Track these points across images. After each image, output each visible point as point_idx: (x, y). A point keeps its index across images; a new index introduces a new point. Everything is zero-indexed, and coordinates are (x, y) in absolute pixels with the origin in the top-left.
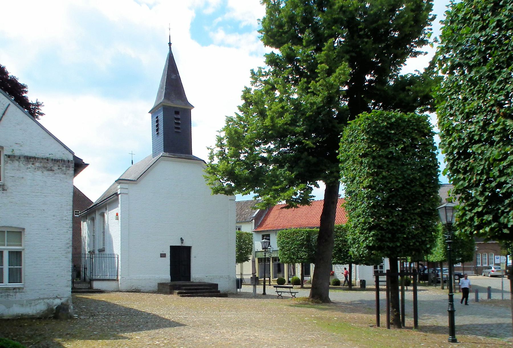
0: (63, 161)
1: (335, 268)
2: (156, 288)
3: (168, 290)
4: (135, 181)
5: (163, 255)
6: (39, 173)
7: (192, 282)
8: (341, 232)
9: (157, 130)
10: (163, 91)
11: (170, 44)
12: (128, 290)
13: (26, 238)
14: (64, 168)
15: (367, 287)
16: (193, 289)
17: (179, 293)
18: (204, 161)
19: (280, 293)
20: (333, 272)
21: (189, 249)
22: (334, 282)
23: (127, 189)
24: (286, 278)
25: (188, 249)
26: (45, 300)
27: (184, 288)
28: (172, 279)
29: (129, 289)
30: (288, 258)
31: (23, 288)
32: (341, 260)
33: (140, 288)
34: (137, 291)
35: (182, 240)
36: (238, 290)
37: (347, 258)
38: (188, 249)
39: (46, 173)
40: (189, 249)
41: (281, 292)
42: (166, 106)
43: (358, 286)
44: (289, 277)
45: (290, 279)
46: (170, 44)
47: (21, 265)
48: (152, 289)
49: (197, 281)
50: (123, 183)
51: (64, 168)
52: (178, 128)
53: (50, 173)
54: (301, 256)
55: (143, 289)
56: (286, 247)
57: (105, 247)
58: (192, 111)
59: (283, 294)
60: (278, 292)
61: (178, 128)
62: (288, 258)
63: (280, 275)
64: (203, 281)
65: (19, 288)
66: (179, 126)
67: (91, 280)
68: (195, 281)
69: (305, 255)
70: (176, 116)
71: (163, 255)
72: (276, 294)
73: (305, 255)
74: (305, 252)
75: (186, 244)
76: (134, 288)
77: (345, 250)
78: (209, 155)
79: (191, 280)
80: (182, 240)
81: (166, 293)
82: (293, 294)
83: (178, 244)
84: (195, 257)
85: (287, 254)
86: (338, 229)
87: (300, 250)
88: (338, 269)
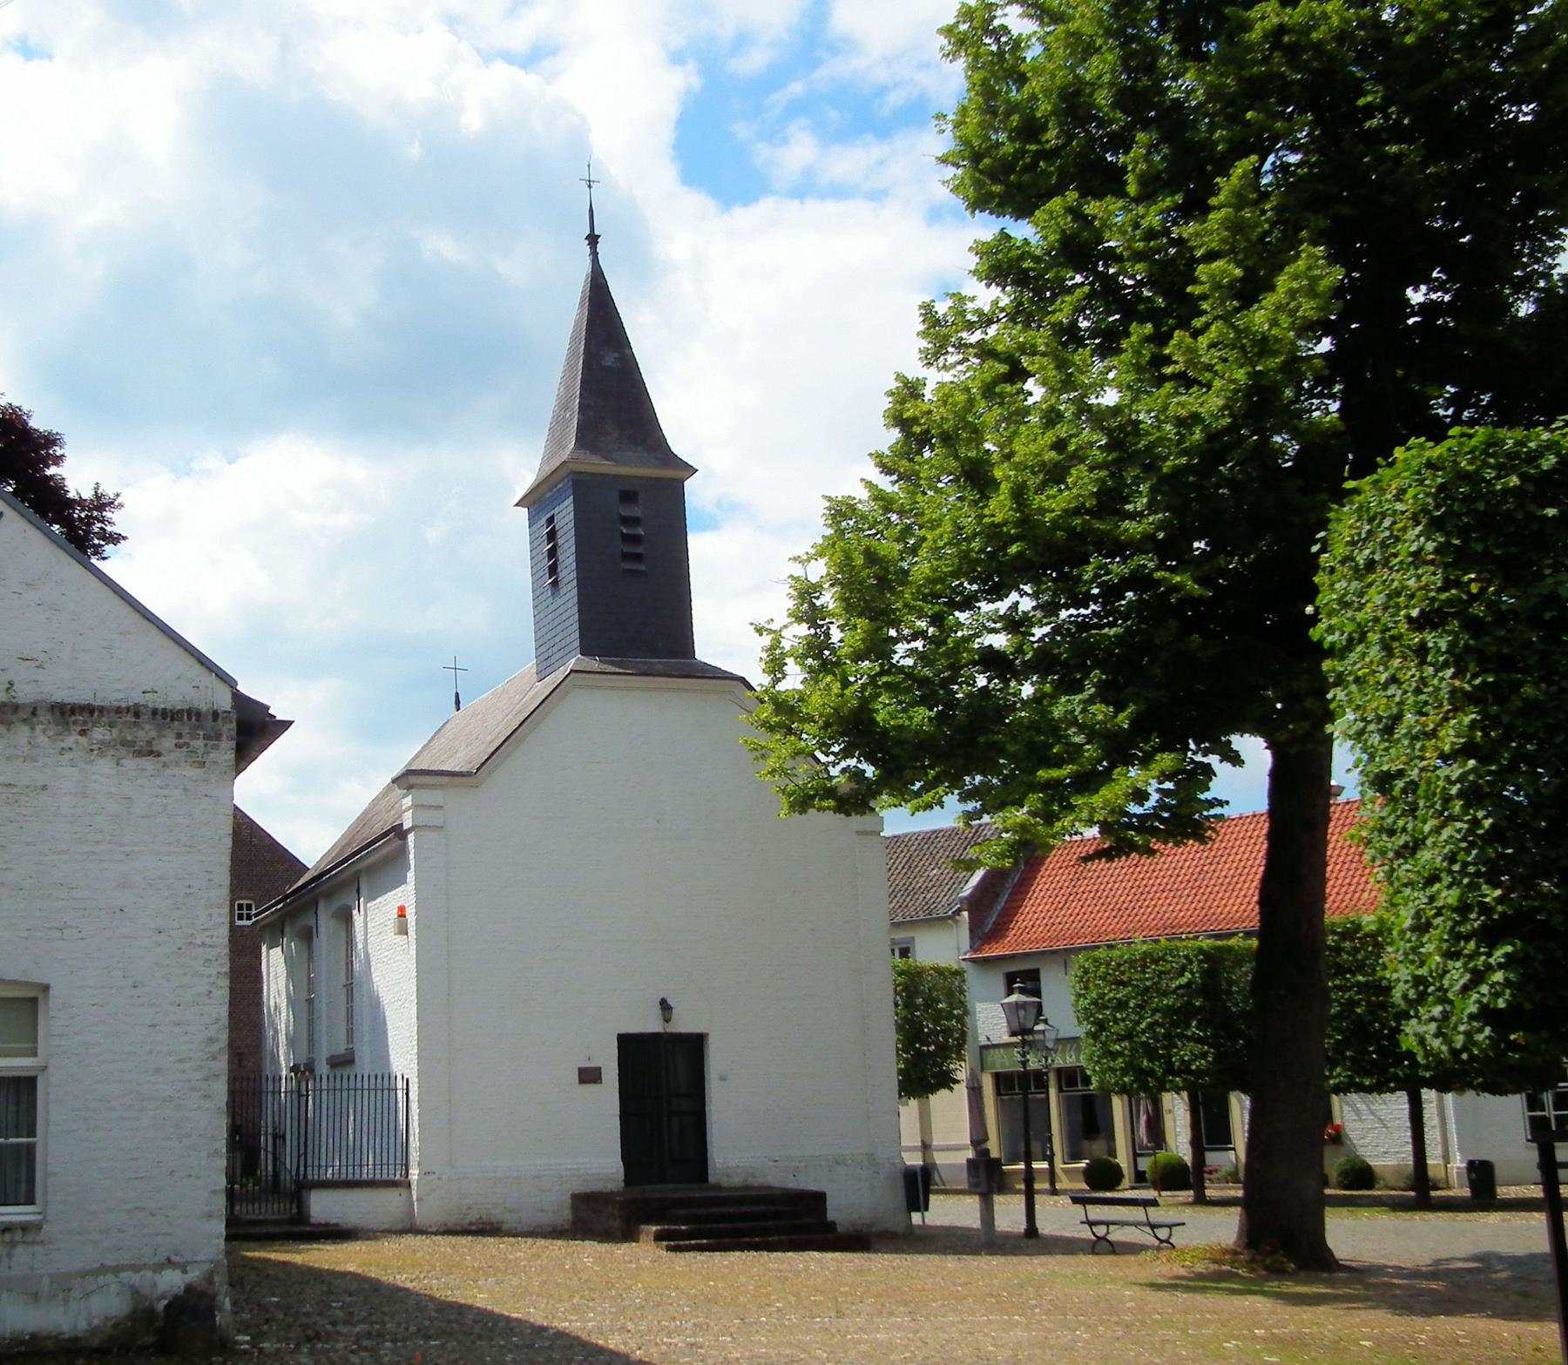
0: (194, 714)
2: (565, 1216)
4: (468, 774)
5: (589, 1076)
6: (104, 766)
7: (717, 1187)
8: (1356, 950)
9: (553, 570)
11: (593, 239)
12: (450, 1225)
13: (53, 1022)
14: (199, 743)
15: (1504, 1192)
17: (659, 1237)
18: (743, 680)
20: (1337, 1129)
21: (696, 1043)
24: (1123, 1159)
26: (124, 1276)
28: (628, 1180)
29: (451, 1221)
30: (1124, 1071)
31: (37, 1227)
32: (1369, 1074)
33: (497, 1214)
34: (487, 1229)
35: (665, 1006)
36: (916, 1218)
39: (131, 763)
40: (696, 1043)
41: (1108, 1224)
44: (1136, 1155)
45: (1145, 1164)
46: (593, 239)
48: (546, 1219)
49: (737, 1181)
50: (423, 786)
51: (199, 743)
52: (638, 557)
53: (148, 763)
54: (1183, 1061)
55: (509, 1220)
57: (356, 1046)
59: (1117, 1235)
60: (1091, 1224)
61: (638, 557)
62: (1124, 1071)
63: (1098, 1148)
64: (760, 1180)
65: (25, 1228)
66: (640, 550)
67: (303, 1186)
68: (725, 1182)
69: (1204, 1055)
71: (589, 1076)
72: (1086, 1233)
73: (1204, 1055)
74: (1199, 1040)
75: (684, 1024)
76: (473, 1216)
78: (764, 655)
79: (712, 1179)
80: (665, 1006)
82: (1163, 1233)
83: (651, 1024)
84: (723, 1078)
87: (1182, 1037)
88: (1357, 1112)
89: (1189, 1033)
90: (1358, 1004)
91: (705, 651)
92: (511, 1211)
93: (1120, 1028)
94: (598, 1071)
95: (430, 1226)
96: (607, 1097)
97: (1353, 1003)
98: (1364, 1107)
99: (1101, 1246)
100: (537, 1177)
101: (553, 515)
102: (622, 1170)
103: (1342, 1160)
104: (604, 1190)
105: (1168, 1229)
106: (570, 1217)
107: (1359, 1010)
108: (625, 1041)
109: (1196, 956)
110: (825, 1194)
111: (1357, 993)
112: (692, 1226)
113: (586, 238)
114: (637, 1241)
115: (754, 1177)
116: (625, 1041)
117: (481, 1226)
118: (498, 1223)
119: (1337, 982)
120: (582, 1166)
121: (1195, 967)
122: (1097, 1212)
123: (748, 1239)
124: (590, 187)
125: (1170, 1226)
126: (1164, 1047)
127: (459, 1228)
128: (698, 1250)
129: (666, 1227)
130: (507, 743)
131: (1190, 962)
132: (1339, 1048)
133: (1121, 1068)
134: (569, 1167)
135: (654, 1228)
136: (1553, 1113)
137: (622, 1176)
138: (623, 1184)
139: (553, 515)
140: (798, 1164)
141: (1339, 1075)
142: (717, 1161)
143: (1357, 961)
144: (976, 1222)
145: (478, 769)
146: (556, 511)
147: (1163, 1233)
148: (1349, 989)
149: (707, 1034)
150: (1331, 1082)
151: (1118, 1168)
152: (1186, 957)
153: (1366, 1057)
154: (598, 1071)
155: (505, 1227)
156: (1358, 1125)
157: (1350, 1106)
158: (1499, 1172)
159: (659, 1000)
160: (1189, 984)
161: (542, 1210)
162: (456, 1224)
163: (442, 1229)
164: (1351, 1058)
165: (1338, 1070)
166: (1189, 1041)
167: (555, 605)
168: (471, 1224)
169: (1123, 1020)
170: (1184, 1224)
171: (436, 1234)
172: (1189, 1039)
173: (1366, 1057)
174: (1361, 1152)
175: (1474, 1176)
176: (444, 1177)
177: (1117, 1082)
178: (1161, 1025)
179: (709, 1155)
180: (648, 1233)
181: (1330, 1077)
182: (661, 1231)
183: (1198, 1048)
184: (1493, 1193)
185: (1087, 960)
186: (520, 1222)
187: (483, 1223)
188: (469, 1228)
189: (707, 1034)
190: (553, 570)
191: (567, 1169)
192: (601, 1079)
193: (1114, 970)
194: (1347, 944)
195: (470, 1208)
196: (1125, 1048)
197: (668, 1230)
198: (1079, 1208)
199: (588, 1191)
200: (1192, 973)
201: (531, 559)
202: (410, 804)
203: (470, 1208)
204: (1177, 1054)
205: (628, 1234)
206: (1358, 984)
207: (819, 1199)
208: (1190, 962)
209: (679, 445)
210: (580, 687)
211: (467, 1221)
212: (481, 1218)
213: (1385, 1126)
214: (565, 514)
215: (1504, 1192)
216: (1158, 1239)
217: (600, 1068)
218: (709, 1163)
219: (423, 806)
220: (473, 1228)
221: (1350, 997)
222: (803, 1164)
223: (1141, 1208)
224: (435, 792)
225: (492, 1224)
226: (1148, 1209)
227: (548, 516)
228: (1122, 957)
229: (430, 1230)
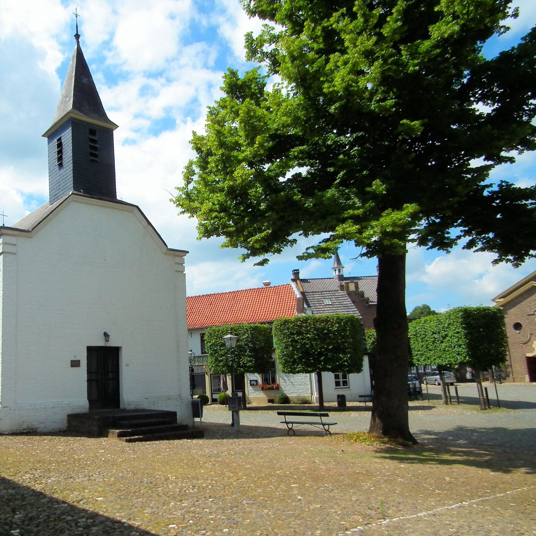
1: (280, 379)
2: (63, 424)
3: (95, 429)
4: (28, 231)
5: (75, 364)
7: (124, 410)
8: (307, 327)
9: (60, 159)
10: (69, 100)
11: (77, 36)
12: (14, 431)
15: (348, 404)
16: (146, 425)
17: (120, 435)
18: (137, 207)
19: (290, 426)
20: (278, 385)
22: (281, 399)
23: (15, 245)
24: (208, 394)
25: (115, 352)
27: (126, 422)
29: (15, 428)
30: (223, 366)
32: (309, 367)
33: (35, 425)
34: (31, 432)
35: (106, 335)
36: (197, 420)
37: (319, 364)
38: (115, 352)
41: (292, 423)
42: (77, 119)
43: (316, 403)
44: (212, 394)
45: (215, 396)
46: (77, 36)
47: (336, 381)
49: (132, 407)
50: (7, 235)
54: (244, 363)
55: (41, 428)
56: (221, 350)
58: (114, 132)
59: (296, 427)
60: (287, 423)
62: (223, 366)
63: (199, 391)
68: (128, 408)
69: (251, 361)
70: (91, 137)
71: (75, 364)
72: (285, 426)
73: (251, 361)
74: (250, 356)
75: (113, 343)
76: (25, 426)
77: (315, 351)
78: (185, 171)
79: (122, 406)
80: (106, 335)
81: (90, 435)
82: (326, 427)
83: (100, 342)
84: (127, 365)
85: (221, 361)
86: (302, 322)
87: (244, 355)
88: (285, 380)
89: (246, 354)
90: (307, 344)
91: (119, 198)
92: (41, 423)
93: (222, 352)
94: (79, 361)
95: (6, 431)
96: (82, 372)
97: (305, 344)
98: (286, 378)
99: (291, 433)
100: (53, 407)
101: (61, 137)
102: (88, 404)
103: (280, 395)
104: (81, 413)
105: (328, 426)
106: (67, 425)
107: (307, 346)
108: (90, 349)
109: (249, 329)
110: (176, 412)
111: (307, 340)
112: (133, 429)
113: (75, 36)
114: (107, 437)
115: (139, 405)
116: (90, 349)
117: (28, 430)
118: (36, 428)
119: (301, 337)
120: (72, 402)
121: (249, 332)
122: (289, 418)
123: (158, 435)
124: (76, 17)
125: (329, 425)
126: (237, 358)
127: (18, 432)
128: (140, 441)
129: (122, 430)
130: (44, 220)
131: (248, 331)
132: (300, 358)
133: (222, 366)
134: (67, 403)
135: (118, 431)
136: (342, 380)
137: (88, 406)
138: (88, 410)
139: (61, 137)
140: (154, 400)
141: (300, 367)
142: (125, 399)
143: (307, 330)
144: (199, 421)
145: (32, 230)
146: (63, 134)
147: (326, 427)
148: (305, 339)
149: (121, 347)
150: (297, 369)
151: (207, 397)
152: (246, 329)
153: (310, 362)
154: (79, 361)
155: (39, 430)
156: (284, 384)
157: (282, 378)
158: (347, 397)
159: (103, 332)
160: (248, 337)
161: (55, 422)
162: (17, 430)
163: (11, 432)
164: (304, 362)
165: (300, 365)
166: (246, 357)
167: (60, 173)
168: (24, 429)
169: (223, 350)
170: (336, 424)
171: (7, 435)
172: (246, 356)
173: (310, 362)
174: (285, 392)
175: (339, 400)
176: (12, 409)
177: (220, 370)
178: (237, 351)
179: (120, 396)
180: (113, 433)
181: (296, 368)
182: (121, 432)
183: (249, 359)
184: (345, 404)
185: (211, 330)
186: (45, 428)
187: (29, 429)
188: (23, 431)
189: (121, 347)
190: (60, 159)
191: (66, 404)
192: (80, 365)
193: (221, 334)
194: (304, 324)
195: (23, 423)
196: (223, 359)
197: (124, 432)
198: (282, 417)
199: (74, 413)
200: (248, 334)
201: (49, 157)
202: (2, 242)
203: (23, 423)
204: (242, 361)
205: (102, 433)
206: (308, 337)
207: (174, 414)
208: (248, 331)
209: (111, 116)
210: (75, 201)
211: (22, 428)
212: (28, 427)
213: (293, 384)
214: (67, 136)
215: (348, 404)
216: (325, 429)
217: (79, 361)
218: (121, 399)
219: (7, 244)
220: (25, 431)
221: (305, 342)
222: (156, 400)
223: (319, 417)
224: (13, 238)
225: (33, 429)
226: (286, 416)
227: (58, 138)
228: (223, 329)
229: (6, 433)
